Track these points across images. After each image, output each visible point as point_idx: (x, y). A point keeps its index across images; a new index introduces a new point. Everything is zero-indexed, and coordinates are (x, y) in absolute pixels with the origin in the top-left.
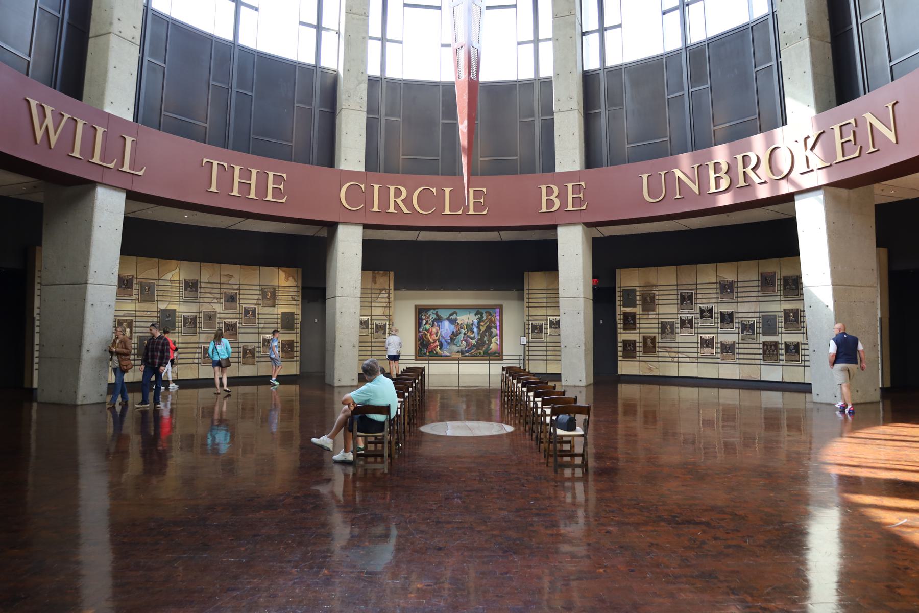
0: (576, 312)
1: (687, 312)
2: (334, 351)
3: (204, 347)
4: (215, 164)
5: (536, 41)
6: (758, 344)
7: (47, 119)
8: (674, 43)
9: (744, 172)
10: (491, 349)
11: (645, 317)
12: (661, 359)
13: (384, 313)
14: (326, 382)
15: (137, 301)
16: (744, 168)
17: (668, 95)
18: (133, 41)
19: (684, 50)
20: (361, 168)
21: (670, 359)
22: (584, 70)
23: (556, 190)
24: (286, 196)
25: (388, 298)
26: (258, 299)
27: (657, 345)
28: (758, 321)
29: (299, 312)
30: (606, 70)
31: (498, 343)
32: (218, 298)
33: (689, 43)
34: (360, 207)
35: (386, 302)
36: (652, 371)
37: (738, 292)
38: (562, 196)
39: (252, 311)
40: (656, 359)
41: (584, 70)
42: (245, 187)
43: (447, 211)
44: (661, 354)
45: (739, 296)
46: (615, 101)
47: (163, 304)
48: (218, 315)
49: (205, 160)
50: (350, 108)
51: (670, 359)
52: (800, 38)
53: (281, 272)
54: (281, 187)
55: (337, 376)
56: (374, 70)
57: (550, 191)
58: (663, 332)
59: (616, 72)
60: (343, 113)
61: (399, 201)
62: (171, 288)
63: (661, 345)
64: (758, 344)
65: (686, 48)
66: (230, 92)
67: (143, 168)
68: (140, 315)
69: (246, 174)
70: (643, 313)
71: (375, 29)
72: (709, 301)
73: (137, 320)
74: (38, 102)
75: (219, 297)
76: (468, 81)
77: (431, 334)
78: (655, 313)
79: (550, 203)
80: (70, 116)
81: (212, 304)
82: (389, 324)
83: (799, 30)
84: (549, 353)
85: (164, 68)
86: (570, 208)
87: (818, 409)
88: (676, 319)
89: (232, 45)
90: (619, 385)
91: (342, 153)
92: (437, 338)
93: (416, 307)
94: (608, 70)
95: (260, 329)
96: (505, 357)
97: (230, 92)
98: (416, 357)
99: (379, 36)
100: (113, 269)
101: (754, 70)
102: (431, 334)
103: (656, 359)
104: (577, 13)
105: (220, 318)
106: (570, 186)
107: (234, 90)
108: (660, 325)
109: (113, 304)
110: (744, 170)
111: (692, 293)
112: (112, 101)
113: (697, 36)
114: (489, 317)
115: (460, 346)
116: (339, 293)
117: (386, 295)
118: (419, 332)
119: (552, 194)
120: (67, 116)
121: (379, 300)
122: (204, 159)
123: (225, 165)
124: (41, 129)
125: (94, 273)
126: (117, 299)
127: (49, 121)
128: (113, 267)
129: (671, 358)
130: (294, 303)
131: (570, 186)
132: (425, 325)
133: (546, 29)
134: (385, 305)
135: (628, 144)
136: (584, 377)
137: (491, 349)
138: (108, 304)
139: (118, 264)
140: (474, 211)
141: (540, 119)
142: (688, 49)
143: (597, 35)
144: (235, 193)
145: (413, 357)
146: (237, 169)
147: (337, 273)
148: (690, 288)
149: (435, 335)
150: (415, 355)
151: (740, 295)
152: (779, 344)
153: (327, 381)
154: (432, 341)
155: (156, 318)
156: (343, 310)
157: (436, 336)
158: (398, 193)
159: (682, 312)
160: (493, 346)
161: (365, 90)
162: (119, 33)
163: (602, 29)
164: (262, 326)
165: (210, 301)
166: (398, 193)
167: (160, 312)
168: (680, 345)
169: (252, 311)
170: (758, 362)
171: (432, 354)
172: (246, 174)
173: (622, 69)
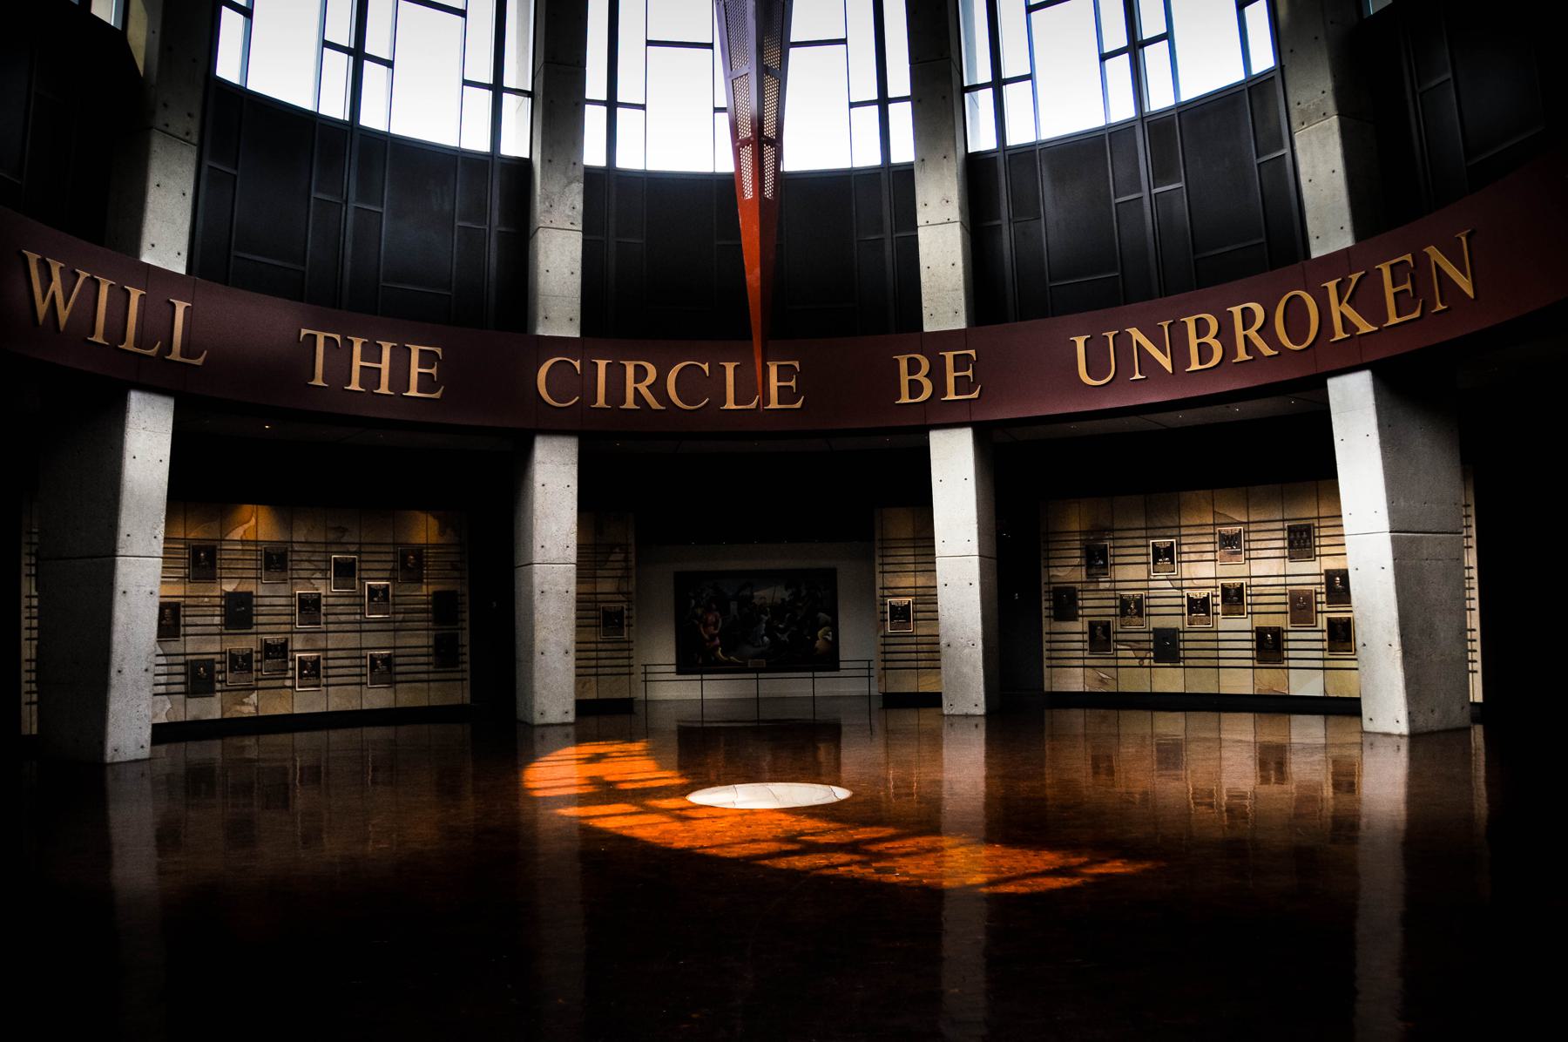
0: (967, 583)
1: (1165, 577)
2: (532, 660)
3: (371, 655)
4: (321, 338)
5: (883, 101)
6: (1214, 632)
7: (53, 283)
8: (1123, 110)
9: (1246, 336)
11: (1092, 587)
12: (1121, 662)
13: (618, 589)
14: (518, 717)
15: (187, 580)
16: (1244, 330)
17: (1116, 197)
18: (187, 138)
19: (1139, 121)
21: (1136, 662)
22: (970, 151)
23: (925, 365)
24: (443, 388)
25: (626, 560)
26: (393, 570)
27: (1113, 637)
28: (1214, 593)
29: (465, 590)
30: (1007, 153)
31: (830, 638)
32: (323, 570)
33: (1147, 110)
34: (574, 401)
35: (621, 569)
36: (1106, 684)
37: (1249, 541)
38: (937, 375)
39: (382, 590)
40: (1112, 662)
41: (970, 151)
42: (370, 376)
43: (730, 405)
44: (1120, 654)
45: (1252, 547)
46: (1027, 206)
47: (230, 583)
48: (323, 601)
49: (304, 332)
50: (553, 225)
51: (1136, 662)
52: (1324, 114)
53: (431, 519)
55: (538, 707)
57: (914, 367)
58: (1123, 614)
59: (1026, 154)
60: (541, 235)
61: (642, 388)
62: (243, 555)
63: (1120, 637)
64: (1214, 632)
65: (1143, 118)
66: (344, 208)
67: (202, 353)
68: (192, 603)
70: (1088, 580)
71: (595, 86)
72: (1202, 556)
73: (187, 613)
74: (39, 257)
75: (323, 567)
76: (760, 202)
78: (1108, 579)
80: (89, 275)
81: (312, 581)
82: (628, 610)
83: (1321, 101)
84: (922, 656)
85: (235, 177)
86: (951, 396)
88: (1145, 589)
89: (348, 128)
91: (540, 305)
92: (717, 632)
94: (1012, 152)
95: (397, 624)
96: (842, 665)
97: (344, 208)
98: (677, 668)
99: (604, 97)
100: (156, 529)
101: (1256, 162)
102: (706, 625)
103: (1112, 662)
105: (326, 605)
107: (352, 205)
108: (1118, 601)
109: (156, 590)
110: (1245, 332)
111: (1172, 543)
112: (154, 242)
115: (759, 646)
116: (537, 558)
117: (621, 557)
119: (1206, 333)
120: (84, 275)
121: (609, 565)
122: (303, 330)
123: (338, 337)
124: (44, 301)
125: (125, 537)
126: (163, 577)
127: (56, 285)
128: (155, 526)
129: (1138, 660)
130: (456, 574)
131: (949, 356)
133: (900, 82)
134: (619, 573)
135: (1050, 280)
136: (983, 699)
138: (149, 589)
139: (164, 520)
140: (779, 403)
141: (894, 236)
142: (1146, 121)
143: (989, 92)
144: (355, 386)
145: (673, 668)
147: (534, 521)
148: (1169, 534)
150: (678, 664)
151: (1253, 545)
152: (1284, 631)
153: (520, 716)
155: (219, 609)
156: (546, 588)
157: (715, 629)
158: (641, 374)
159: (1156, 578)
161: (578, 193)
162: (164, 128)
164: (400, 617)
165: (309, 576)
166: (641, 374)
167: (224, 597)
168: (1221, 636)
169: (382, 590)
170: (189, 601)
173: (1035, 150)
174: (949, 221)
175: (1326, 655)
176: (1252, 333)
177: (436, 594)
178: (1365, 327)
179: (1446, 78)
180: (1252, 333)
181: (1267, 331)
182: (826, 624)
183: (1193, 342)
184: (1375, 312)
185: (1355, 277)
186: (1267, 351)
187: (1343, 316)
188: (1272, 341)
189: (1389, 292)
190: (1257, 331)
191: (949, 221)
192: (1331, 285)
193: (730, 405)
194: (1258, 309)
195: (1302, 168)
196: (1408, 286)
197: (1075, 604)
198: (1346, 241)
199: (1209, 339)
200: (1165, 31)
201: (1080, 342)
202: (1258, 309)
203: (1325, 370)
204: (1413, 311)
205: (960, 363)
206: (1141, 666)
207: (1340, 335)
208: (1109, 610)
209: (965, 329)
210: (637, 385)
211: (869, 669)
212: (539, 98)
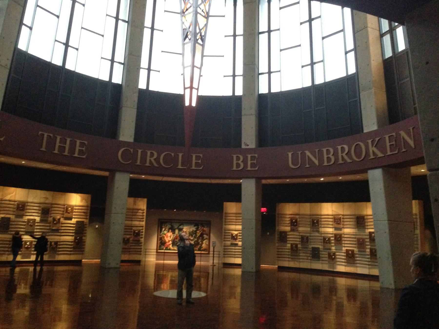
5: (235, 36)
9: (342, 156)
10: (202, 247)
20: (131, 140)
22: (260, 93)
23: (332, 151)
38: (245, 161)
42: (62, 149)
49: (40, 133)
54: (84, 149)
56: (142, 85)
57: (238, 158)
60: (124, 109)
61: (152, 159)
69: (63, 141)
71: (148, 22)
77: (167, 237)
79: (238, 165)
87: (244, 195)
90: (225, 203)
93: (159, 219)
102: (167, 237)
104: (256, 63)
106: (249, 156)
113: (319, 81)
114: (203, 228)
118: (160, 235)
119: (329, 154)
123: (52, 135)
131: (249, 156)
132: (164, 231)
137: (202, 247)
146: (59, 138)
149: (169, 238)
154: (167, 241)
158: (152, 155)
160: (204, 246)
163: (270, 73)
166: (152, 155)
171: (167, 249)
172: (63, 141)
174: (251, 114)
175: (369, 260)
176: (344, 155)
177: (77, 222)
178: (380, 155)
179: (136, 259)
180: (344, 155)
181: (348, 154)
182: (206, 239)
183: (325, 156)
184: (383, 150)
185: (377, 139)
186: (349, 161)
187: (373, 152)
188: (351, 158)
189: (388, 144)
190: (346, 154)
191: (251, 114)
192: (370, 141)
193: (180, 167)
194: (346, 147)
195: (362, 104)
196: (394, 143)
197: (286, 236)
198: (375, 127)
199: (330, 156)
200: (342, 29)
201: (290, 154)
202: (346, 147)
203: (392, 163)
204: (395, 151)
205: (253, 158)
206: (307, 259)
207: (372, 157)
208: (297, 241)
209: (254, 148)
210: (150, 159)
211: (219, 254)
212: (126, 66)
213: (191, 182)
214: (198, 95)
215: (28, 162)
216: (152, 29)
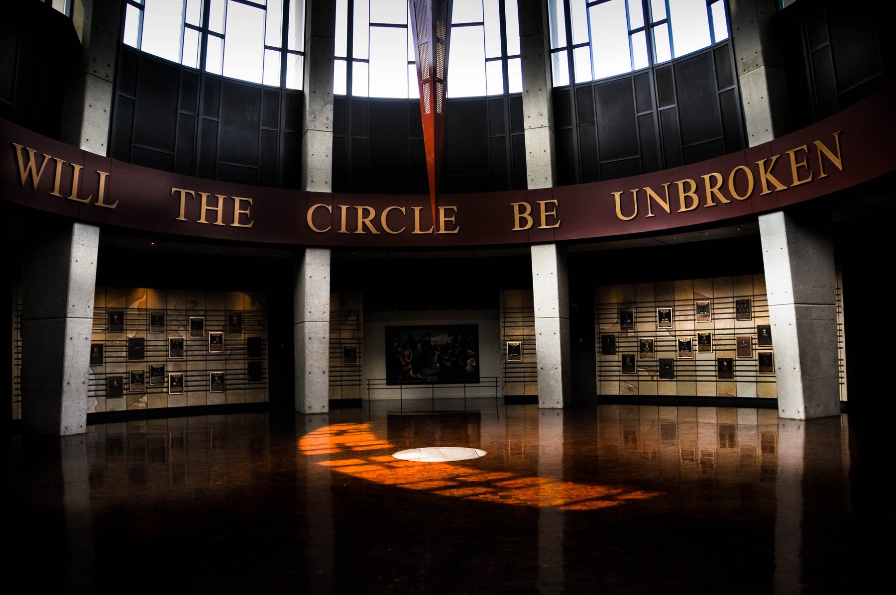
0: (552, 333)
1: (666, 330)
2: (304, 377)
3: (212, 374)
4: (183, 193)
5: (505, 58)
6: (694, 361)
7: (30, 162)
8: (642, 63)
9: (712, 192)
11: (624, 335)
12: (641, 378)
13: (353, 336)
14: (296, 410)
15: (107, 331)
16: (711, 188)
17: (638, 113)
18: (107, 79)
19: (651, 69)
21: (649, 378)
22: (554, 86)
23: (529, 208)
24: (253, 221)
25: (358, 320)
26: (224, 325)
27: (636, 364)
28: (694, 339)
29: (266, 337)
30: (575, 87)
31: (474, 364)
32: (184, 325)
33: (655, 63)
34: (328, 229)
35: (355, 325)
36: (632, 390)
37: (714, 309)
38: (535, 214)
39: (218, 337)
40: (636, 378)
41: (554, 86)
42: (211, 215)
43: (417, 231)
44: (640, 373)
45: (715, 312)
46: (587, 118)
47: (131, 333)
48: (185, 343)
49: (174, 189)
50: (316, 129)
51: (649, 378)
52: (757, 65)
53: (246, 296)
55: (307, 404)
56: (841, 400)
57: (522, 209)
58: (642, 350)
59: (587, 88)
60: (309, 134)
61: (367, 221)
62: (139, 317)
63: (640, 364)
64: (694, 361)
65: (653, 68)
66: (197, 119)
67: (116, 201)
68: (110, 344)
70: (622, 331)
71: (340, 49)
72: (687, 318)
73: (107, 350)
74: (22, 147)
75: (185, 324)
76: (434, 116)
78: (633, 331)
80: (51, 157)
81: (178, 332)
82: (359, 348)
83: (755, 57)
84: (527, 374)
85: (134, 101)
86: (544, 226)
88: (655, 336)
89: (199, 73)
91: (309, 174)
92: (410, 361)
94: (578, 87)
95: (227, 356)
96: (481, 380)
97: (197, 119)
98: (387, 382)
99: (345, 55)
100: (89, 302)
101: (717, 92)
102: (403, 357)
103: (636, 378)
105: (186, 346)
107: (201, 117)
108: (639, 343)
109: (89, 337)
110: (711, 190)
111: (670, 310)
112: (88, 138)
115: (434, 369)
116: (307, 318)
117: (355, 318)
119: (689, 190)
120: (48, 157)
121: (348, 323)
122: (173, 188)
123: (193, 193)
124: (25, 172)
125: (72, 307)
126: (93, 330)
127: (32, 163)
128: (89, 300)
129: (650, 377)
130: (261, 328)
131: (542, 204)
133: (514, 47)
134: (354, 327)
135: (600, 160)
136: (562, 399)
138: (85, 336)
139: (93, 297)
140: (445, 230)
141: (511, 135)
142: (655, 69)
143: (565, 53)
144: (203, 220)
145: (385, 382)
147: (305, 297)
148: (668, 305)
150: (387, 379)
151: (716, 311)
152: (734, 360)
153: (297, 409)
155: (125, 348)
156: (312, 336)
157: (409, 359)
158: (366, 214)
159: (661, 330)
161: (330, 110)
162: (94, 73)
164: (229, 352)
165: (177, 329)
166: (366, 214)
167: (128, 341)
168: (698, 363)
169: (218, 337)
170: (108, 343)
173: (592, 86)
174: (542, 126)
175: (758, 374)
176: (715, 190)
177: (249, 339)
178: (780, 187)
180: (715, 190)
181: (724, 189)
182: (472, 356)
183: (682, 196)
184: (786, 178)
185: (774, 158)
186: (724, 201)
187: (767, 180)
188: (727, 195)
189: (794, 167)
190: (719, 189)
191: (542, 126)
192: (761, 163)
193: (417, 231)
194: (719, 177)
195: (744, 96)
196: (805, 163)
197: (614, 345)
198: (769, 137)
199: (691, 194)
200: (666, 18)
201: (617, 195)
202: (719, 177)
203: (757, 212)
204: (808, 178)
205: (548, 207)
206: (652, 381)
207: (766, 191)
208: (634, 348)
209: (551, 188)
210: (364, 220)
211: (497, 382)
212: (308, 56)
213: (200, 417)
214: (483, 26)
215: (517, 448)
216: (350, 59)
